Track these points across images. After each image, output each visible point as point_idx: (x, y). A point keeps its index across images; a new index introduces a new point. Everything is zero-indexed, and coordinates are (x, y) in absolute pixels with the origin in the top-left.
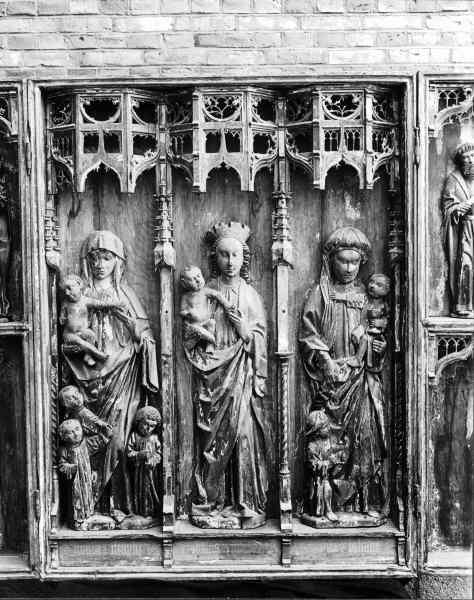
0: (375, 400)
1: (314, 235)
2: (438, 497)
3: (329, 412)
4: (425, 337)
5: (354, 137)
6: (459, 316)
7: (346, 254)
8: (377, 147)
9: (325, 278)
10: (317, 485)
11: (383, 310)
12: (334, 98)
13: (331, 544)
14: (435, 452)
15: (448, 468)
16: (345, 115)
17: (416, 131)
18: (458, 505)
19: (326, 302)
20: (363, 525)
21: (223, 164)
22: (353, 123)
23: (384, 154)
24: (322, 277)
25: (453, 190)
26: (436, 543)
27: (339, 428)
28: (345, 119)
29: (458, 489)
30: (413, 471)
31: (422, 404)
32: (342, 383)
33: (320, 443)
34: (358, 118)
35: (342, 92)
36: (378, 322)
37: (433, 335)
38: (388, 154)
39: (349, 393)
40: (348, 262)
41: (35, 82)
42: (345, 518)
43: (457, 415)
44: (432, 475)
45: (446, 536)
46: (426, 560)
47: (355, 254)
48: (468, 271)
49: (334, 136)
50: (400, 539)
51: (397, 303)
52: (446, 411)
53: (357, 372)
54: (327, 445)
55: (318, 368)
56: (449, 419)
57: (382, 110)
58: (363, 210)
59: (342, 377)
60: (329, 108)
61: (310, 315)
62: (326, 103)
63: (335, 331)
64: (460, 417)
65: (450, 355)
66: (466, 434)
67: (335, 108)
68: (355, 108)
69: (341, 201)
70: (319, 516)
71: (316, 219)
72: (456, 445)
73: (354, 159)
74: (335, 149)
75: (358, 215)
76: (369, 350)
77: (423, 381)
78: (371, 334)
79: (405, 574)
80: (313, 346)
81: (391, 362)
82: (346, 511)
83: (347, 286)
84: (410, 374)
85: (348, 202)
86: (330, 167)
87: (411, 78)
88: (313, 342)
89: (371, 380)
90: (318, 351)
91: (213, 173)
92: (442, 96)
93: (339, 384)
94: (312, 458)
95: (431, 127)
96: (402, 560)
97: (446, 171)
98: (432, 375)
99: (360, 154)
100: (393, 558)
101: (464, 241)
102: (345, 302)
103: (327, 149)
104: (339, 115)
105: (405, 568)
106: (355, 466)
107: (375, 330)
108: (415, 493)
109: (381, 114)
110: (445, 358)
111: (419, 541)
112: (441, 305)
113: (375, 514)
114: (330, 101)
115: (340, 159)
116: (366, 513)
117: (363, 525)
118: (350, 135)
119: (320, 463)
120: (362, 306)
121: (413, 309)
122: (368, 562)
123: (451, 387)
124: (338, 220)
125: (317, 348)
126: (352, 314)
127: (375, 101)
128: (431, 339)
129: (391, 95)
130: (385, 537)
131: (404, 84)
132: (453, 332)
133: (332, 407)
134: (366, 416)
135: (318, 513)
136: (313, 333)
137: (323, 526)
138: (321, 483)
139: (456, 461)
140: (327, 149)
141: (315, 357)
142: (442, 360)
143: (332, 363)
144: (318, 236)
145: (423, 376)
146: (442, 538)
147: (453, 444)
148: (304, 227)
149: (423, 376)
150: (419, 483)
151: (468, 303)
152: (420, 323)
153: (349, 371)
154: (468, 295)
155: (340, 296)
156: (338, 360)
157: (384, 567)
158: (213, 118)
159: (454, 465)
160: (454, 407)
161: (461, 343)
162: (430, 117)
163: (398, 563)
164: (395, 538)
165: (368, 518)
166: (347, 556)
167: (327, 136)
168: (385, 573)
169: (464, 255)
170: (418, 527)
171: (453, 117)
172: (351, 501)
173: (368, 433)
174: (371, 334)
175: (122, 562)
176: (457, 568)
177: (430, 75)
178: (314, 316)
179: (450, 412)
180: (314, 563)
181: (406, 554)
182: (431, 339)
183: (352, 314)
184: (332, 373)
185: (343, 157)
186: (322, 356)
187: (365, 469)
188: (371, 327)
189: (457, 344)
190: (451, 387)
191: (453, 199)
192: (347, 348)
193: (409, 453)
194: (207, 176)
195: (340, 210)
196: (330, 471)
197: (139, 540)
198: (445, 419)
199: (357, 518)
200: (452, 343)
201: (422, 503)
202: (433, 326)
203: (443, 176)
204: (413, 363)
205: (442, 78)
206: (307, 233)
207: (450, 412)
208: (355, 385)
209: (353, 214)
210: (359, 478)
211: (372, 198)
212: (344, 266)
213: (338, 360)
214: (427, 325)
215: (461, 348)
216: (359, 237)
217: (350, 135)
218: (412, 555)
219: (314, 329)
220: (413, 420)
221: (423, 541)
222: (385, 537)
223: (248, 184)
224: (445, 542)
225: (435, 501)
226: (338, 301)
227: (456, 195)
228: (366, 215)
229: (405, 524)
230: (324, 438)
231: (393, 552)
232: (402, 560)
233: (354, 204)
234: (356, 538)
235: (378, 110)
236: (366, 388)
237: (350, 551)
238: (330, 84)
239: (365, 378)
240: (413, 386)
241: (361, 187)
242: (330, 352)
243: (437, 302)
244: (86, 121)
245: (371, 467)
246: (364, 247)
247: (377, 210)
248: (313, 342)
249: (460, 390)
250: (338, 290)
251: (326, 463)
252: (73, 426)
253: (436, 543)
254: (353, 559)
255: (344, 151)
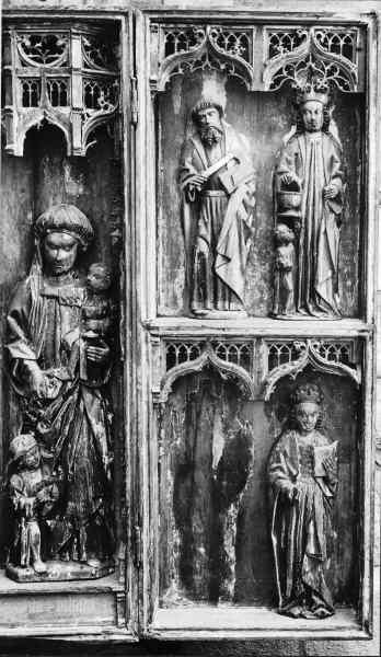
0: (93, 421)
1: (25, 214)
2: (178, 541)
3: (38, 436)
4: (147, 341)
5: (59, 90)
6: (196, 316)
7: (55, 238)
8: (90, 101)
9: (37, 268)
10: (21, 528)
11: (104, 308)
12: (34, 40)
13: (35, 603)
14: (176, 484)
15: (191, 504)
16: (48, 61)
17: (134, 83)
18: (202, 550)
19: (34, 298)
20: (78, 578)
21: (44, 121)
22: (57, 72)
23: (101, 112)
24: (34, 267)
25: (190, 159)
26: (176, 596)
27: (51, 455)
28: (47, 66)
29: (202, 531)
30: (132, 510)
31: (143, 427)
32: (52, 400)
33: (26, 475)
34: (64, 65)
35: (44, 31)
36: (93, 323)
37: (158, 339)
38: (107, 112)
39: (61, 414)
40: (57, 248)
41: (145, 12)
42: (56, 568)
43: (200, 438)
44: (172, 514)
45: (187, 589)
46: (150, 620)
47: (67, 238)
48: (204, 260)
49: (34, 87)
50: (119, 595)
51: (113, 296)
52: (188, 433)
53: (69, 385)
54: (35, 478)
55: (24, 381)
56: (191, 444)
57: (100, 56)
58: (87, 184)
59: (52, 393)
60: (27, 51)
61: (15, 314)
62: (23, 45)
63: (43, 336)
64: (205, 440)
65: (182, 365)
66: (211, 463)
67: (34, 52)
68: (61, 52)
69: (58, 171)
70: (24, 567)
71: (27, 196)
72: (200, 476)
73: (59, 117)
74: (35, 104)
75: (81, 190)
76: (82, 360)
77: (145, 398)
78: (85, 338)
79: (123, 638)
80: (16, 354)
81: (105, 374)
82: (62, 559)
83: (62, 279)
84: (128, 387)
85: (67, 173)
86: (30, 125)
87: (126, 14)
88: (18, 348)
89: (88, 397)
90: (21, 360)
91: (32, 134)
92: (170, 38)
93: (47, 402)
94: (14, 494)
95: (152, 78)
96: (121, 621)
97: (185, 135)
98: (157, 390)
99: (65, 110)
100: (112, 618)
101: (201, 223)
102: (57, 298)
103: (26, 104)
104: (40, 61)
105: (125, 631)
106: (70, 504)
107: (91, 334)
108: (135, 537)
109: (98, 62)
110: (174, 368)
111: (141, 597)
112: (181, 302)
113: (94, 563)
114: (28, 43)
115: (41, 117)
116: (85, 563)
117: (78, 578)
118: (55, 86)
119: (23, 501)
120: (80, 303)
121: (131, 306)
122: (81, 624)
123: (193, 404)
124: (55, 195)
125: (23, 356)
126: (66, 313)
127: (87, 43)
128: (155, 345)
129: (105, 35)
130: (100, 593)
131: (119, 23)
132: (182, 336)
133: (43, 430)
134: (81, 442)
135: (23, 562)
136: (18, 338)
137: (27, 579)
138: (26, 525)
139: (199, 496)
140: (26, 104)
141: (19, 367)
142: (170, 371)
143: (38, 374)
144: (30, 216)
145: (144, 389)
146: (183, 591)
147: (196, 474)
148: (12, 204)
149: (144, 389)
150: (141, 525)
151: (205, 298)
152: (140, 326)
153: (59, 385)
154: (205, 289)
155: (50, 291)
156: (48, 372)
157: (100, 630)
158: (32, 62)
159: (197, 500)
160: (198, 428)
161: (194, 349)
162: (153, 65)
163: (115, 623)
164: (111, 593)
165: (86, 569)
166: (54, 618)
167: (25, 87)
168: (100, 638)
169: (200, 240)
170: (139, 580)
171: (288, 68)
172: (68, 547)
173: (85, 461)
174: (85, 338)
175: (122, 610)
176: (190, 629)
177: (151, 12)
178: (21, 316)
179: (192, 435)
180: (13, 626)
181: (126, 614)
182: (155, 345)
183: (66, 313)
184: (37, 388)
185: (45, 114)
186: (26, 366)
187: (81, 507)
188: (87, 331)
189: (189, 351)
190: (193, 404)
191: (188, 170)
192: (58, 356)
193: (129, 486)
194: (24, 136)
195: (58, 182)
196: (39, 506)
197: (88, 593)
198: (187, 442)
199: (71, 569)
200: (183, 350)
201: (145, 551)
202: (157, 328)
203: (181, 141)
204: (131, 375)
205: (166, 16)
206: (17, 212)
207: (192, 435)
208: (67, 402)
209: (75, 188)
210: (74, 518)
211: (98, 167)
212: (54, 253)
213: (48, 372)
214: (148, 328)
215: (194, 356)
216: (74, 216)
217: (55, 86)
218: (133, 613)
219: (20, 332)
220: (132, 445)
221: (146, 596)
222: (100, 593)
223: (79, 144)
224: (187, 596)
225: (175, 546)
226: (48, 297)
227: (193, 164)
228: (91, 190)
229: (125, 575)
230: (31, 468)
231: (111, 611)
232: (121, 621)
233: (75, 175)
234: (64, 594)
235: (93, 56)
236: (82, 408)
237: (58, 610)
238: (26, 20)
239: (80, 395)
240: (132, 404)
241: (69, 154)
242: (40, 362)
243: (175, 298)
244: (24, 64)
245: (88, 505)
246: (78, 229)
247: (104, 184)
248: (18, 348)
249: (204, 408)
250: (50, 284)
251: (31, 501)
252: (161, 442)
253: (176, 596)
254: (62, 620)
255: (46, 107)
